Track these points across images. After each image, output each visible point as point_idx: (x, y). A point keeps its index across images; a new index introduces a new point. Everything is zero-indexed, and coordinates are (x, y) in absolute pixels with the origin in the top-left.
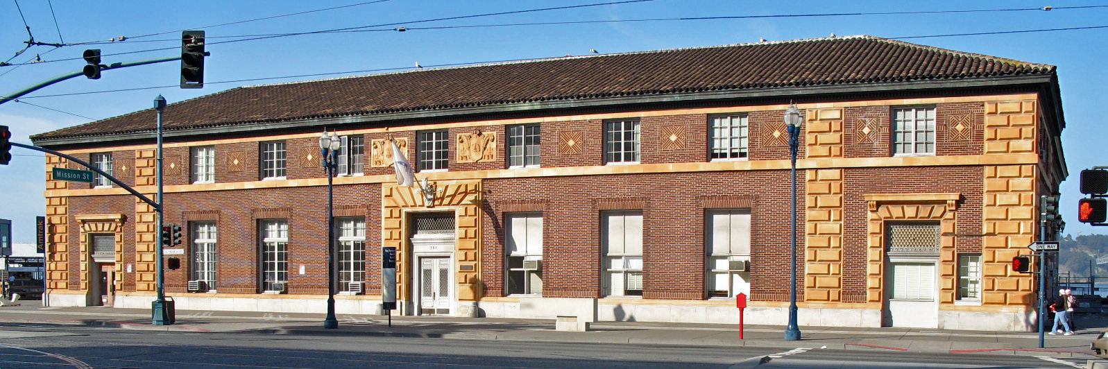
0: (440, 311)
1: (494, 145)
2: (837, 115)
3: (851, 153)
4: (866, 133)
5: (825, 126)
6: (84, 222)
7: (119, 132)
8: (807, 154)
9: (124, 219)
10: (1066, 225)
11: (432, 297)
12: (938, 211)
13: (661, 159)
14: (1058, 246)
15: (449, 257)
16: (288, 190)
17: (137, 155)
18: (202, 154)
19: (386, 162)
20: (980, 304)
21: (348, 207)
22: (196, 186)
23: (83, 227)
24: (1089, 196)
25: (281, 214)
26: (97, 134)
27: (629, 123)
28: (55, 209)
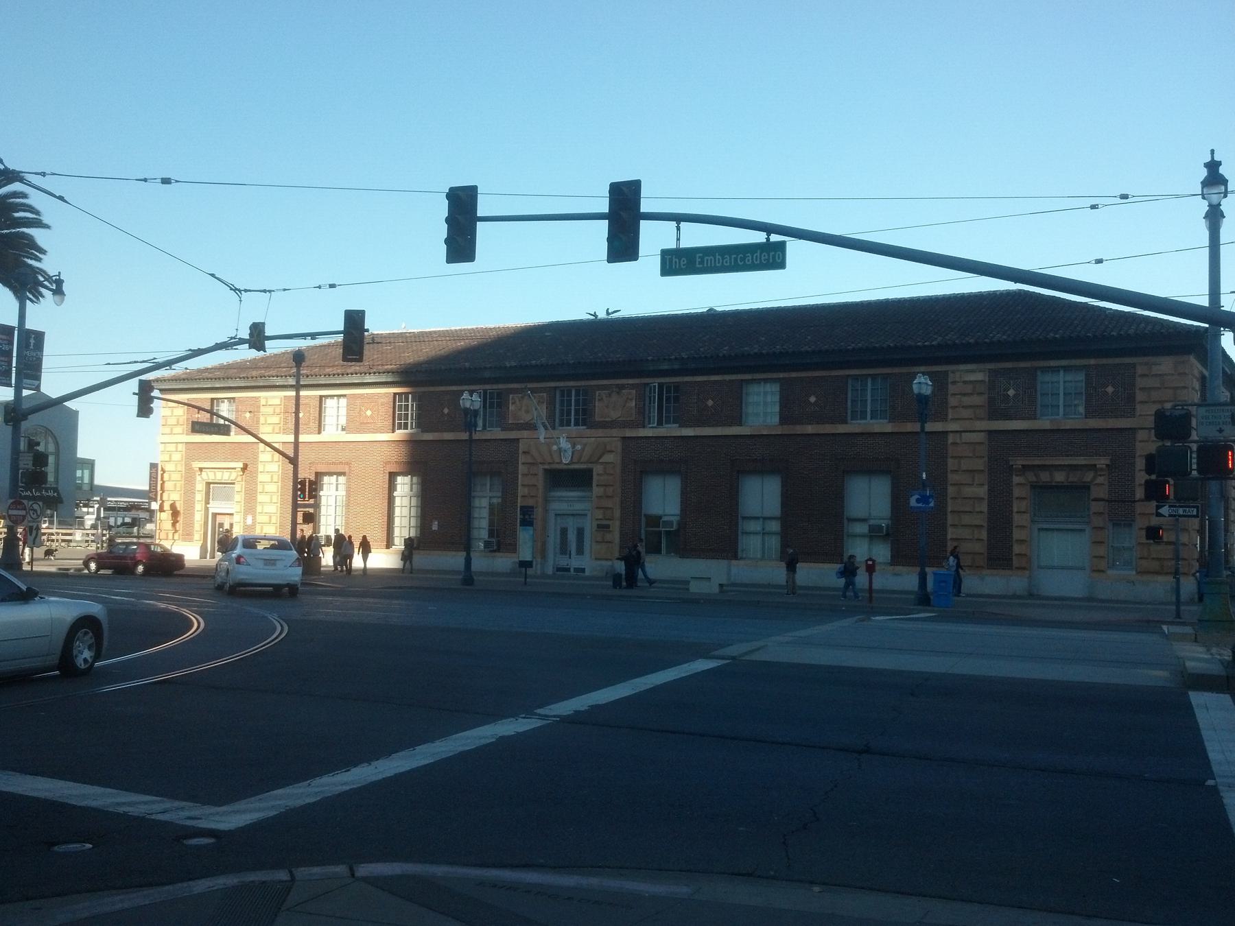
0: (577, 570)
2: (277, 402)
3: (994, 414)
5: (969, 389)
6: (201, 469)
7: (244, 378)
8: (950, 417)
9: (244, 468)
11: (568, 556)
12: (1089, 477)
14: (1198, 511)
15: (586, 515)
17: (263, 402)
18: (330, 404)
19: (526, 418)
20: (1134, 573)
22: (325, 437)
26: (219, 379)
28: (170, 456)
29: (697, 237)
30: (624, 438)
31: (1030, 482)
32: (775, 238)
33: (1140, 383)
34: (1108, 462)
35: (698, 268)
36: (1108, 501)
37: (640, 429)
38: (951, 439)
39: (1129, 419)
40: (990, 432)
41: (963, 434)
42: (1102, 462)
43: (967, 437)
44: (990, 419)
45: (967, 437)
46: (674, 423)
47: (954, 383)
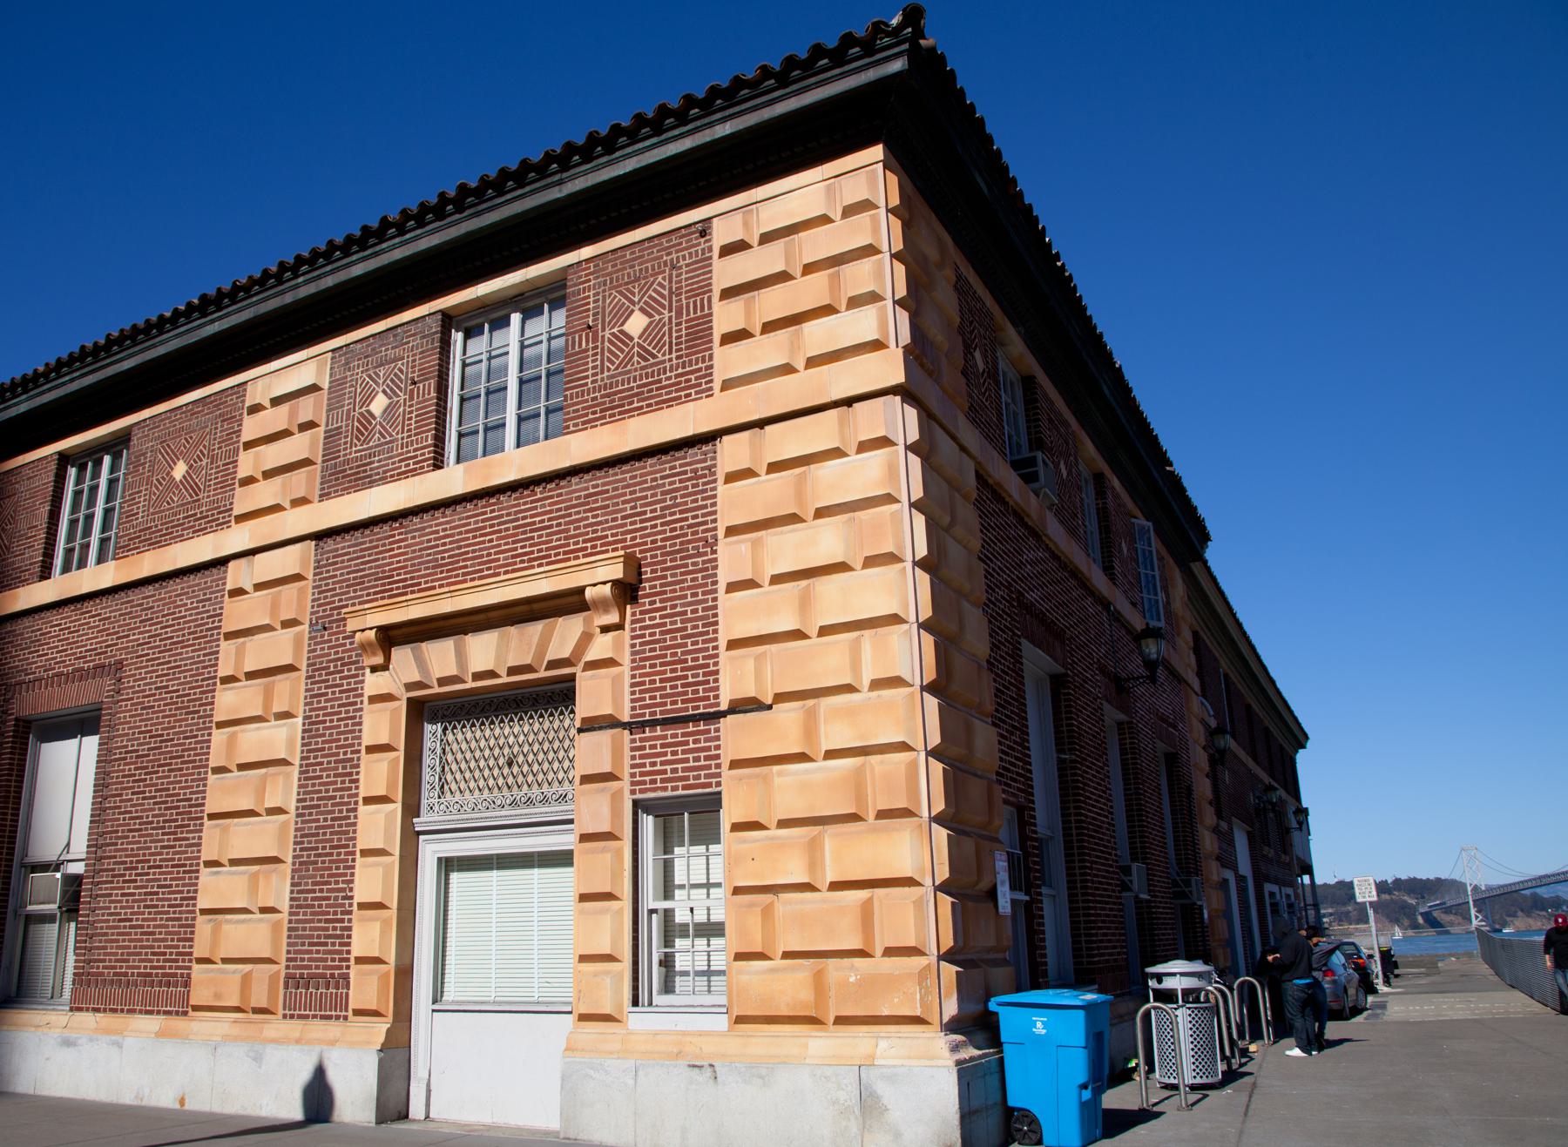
12: (564, 634)
36: (632, 727)
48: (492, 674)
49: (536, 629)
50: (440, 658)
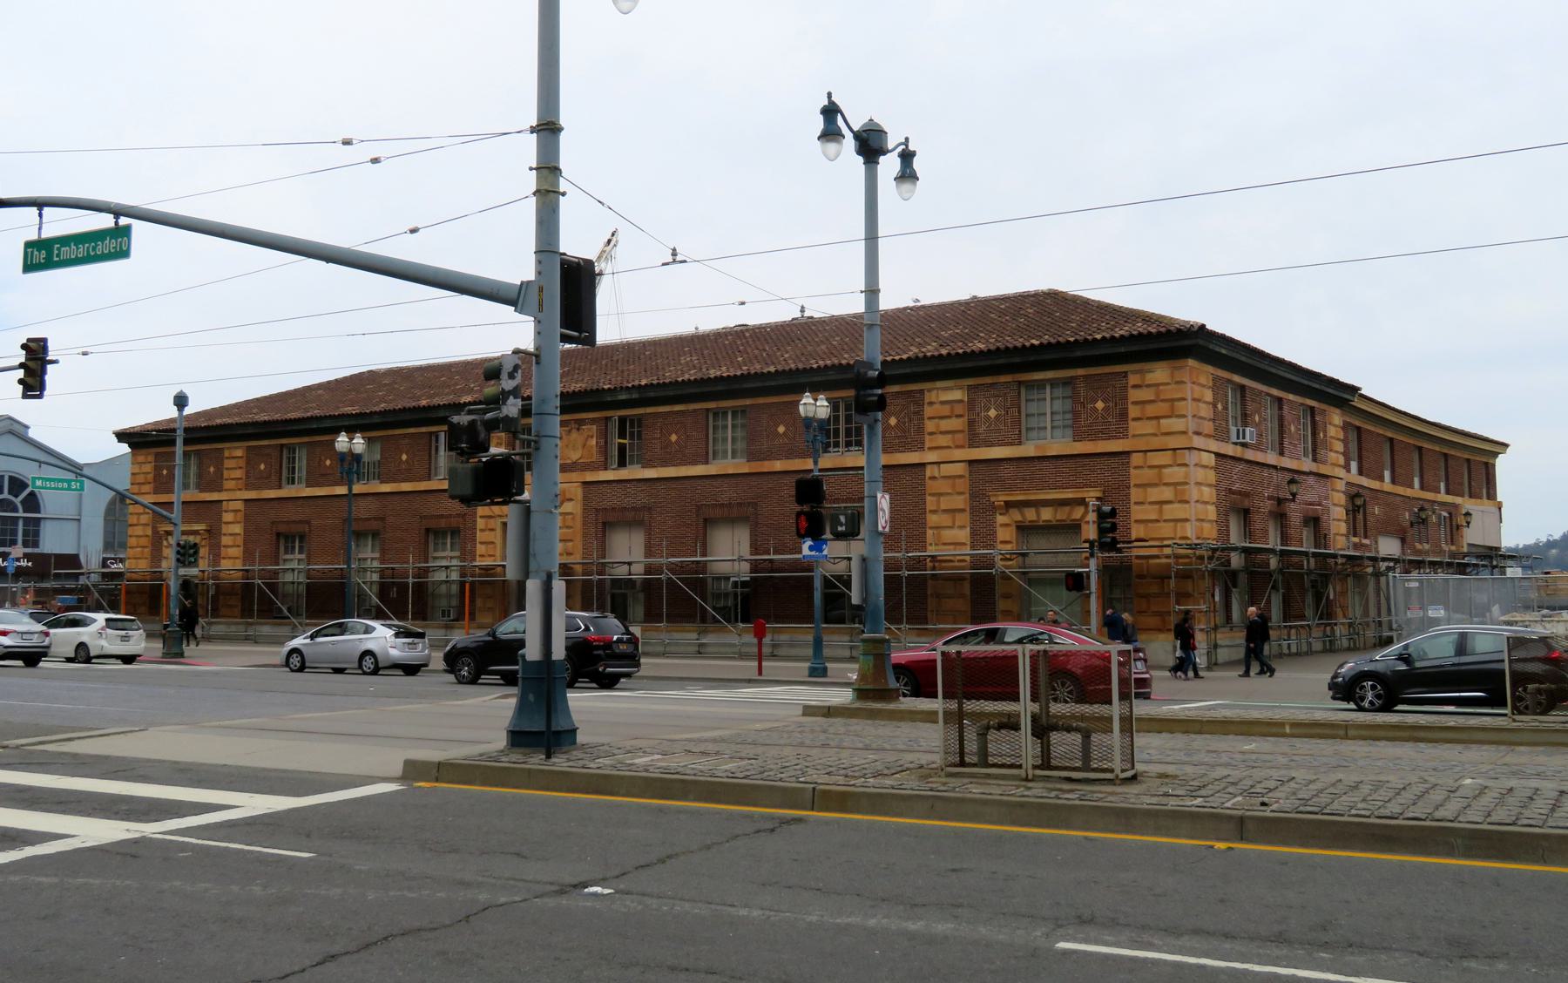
1: (593, 442)
3: (973, 441)
4: (993, 416)
5: (946, 410)
8: (927, 445)
10: (1473, 516)
12: (1078, 513)
13: (770, 456)
16: (300, 502)
21: (442, 516)
23: (166, 539)
24: (806, 508)
25: (375, 525)
27: (292, 449)
29: (61, 223)
30: (585, 483)
31: (1016, 522)
32: (123, 221)
33: (1134, 395)
34: (1099, 494)
35: (56, 261)
37: (601, 472)
38: (929, 471)
39: (1121, 441)
40: (971, 462)
41: (942, 465)
42: (1092, 494)
43: (947, 469)
44: (971, 446)
45: (947, 469)
46: (637, 464)
47: (931, 403)
48: (1050, 521)
49: (1067, 509)
50: (1030, 514)
